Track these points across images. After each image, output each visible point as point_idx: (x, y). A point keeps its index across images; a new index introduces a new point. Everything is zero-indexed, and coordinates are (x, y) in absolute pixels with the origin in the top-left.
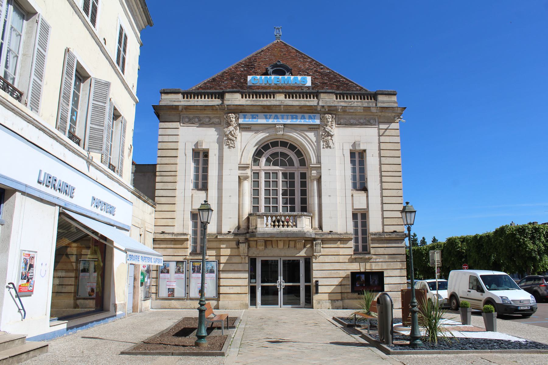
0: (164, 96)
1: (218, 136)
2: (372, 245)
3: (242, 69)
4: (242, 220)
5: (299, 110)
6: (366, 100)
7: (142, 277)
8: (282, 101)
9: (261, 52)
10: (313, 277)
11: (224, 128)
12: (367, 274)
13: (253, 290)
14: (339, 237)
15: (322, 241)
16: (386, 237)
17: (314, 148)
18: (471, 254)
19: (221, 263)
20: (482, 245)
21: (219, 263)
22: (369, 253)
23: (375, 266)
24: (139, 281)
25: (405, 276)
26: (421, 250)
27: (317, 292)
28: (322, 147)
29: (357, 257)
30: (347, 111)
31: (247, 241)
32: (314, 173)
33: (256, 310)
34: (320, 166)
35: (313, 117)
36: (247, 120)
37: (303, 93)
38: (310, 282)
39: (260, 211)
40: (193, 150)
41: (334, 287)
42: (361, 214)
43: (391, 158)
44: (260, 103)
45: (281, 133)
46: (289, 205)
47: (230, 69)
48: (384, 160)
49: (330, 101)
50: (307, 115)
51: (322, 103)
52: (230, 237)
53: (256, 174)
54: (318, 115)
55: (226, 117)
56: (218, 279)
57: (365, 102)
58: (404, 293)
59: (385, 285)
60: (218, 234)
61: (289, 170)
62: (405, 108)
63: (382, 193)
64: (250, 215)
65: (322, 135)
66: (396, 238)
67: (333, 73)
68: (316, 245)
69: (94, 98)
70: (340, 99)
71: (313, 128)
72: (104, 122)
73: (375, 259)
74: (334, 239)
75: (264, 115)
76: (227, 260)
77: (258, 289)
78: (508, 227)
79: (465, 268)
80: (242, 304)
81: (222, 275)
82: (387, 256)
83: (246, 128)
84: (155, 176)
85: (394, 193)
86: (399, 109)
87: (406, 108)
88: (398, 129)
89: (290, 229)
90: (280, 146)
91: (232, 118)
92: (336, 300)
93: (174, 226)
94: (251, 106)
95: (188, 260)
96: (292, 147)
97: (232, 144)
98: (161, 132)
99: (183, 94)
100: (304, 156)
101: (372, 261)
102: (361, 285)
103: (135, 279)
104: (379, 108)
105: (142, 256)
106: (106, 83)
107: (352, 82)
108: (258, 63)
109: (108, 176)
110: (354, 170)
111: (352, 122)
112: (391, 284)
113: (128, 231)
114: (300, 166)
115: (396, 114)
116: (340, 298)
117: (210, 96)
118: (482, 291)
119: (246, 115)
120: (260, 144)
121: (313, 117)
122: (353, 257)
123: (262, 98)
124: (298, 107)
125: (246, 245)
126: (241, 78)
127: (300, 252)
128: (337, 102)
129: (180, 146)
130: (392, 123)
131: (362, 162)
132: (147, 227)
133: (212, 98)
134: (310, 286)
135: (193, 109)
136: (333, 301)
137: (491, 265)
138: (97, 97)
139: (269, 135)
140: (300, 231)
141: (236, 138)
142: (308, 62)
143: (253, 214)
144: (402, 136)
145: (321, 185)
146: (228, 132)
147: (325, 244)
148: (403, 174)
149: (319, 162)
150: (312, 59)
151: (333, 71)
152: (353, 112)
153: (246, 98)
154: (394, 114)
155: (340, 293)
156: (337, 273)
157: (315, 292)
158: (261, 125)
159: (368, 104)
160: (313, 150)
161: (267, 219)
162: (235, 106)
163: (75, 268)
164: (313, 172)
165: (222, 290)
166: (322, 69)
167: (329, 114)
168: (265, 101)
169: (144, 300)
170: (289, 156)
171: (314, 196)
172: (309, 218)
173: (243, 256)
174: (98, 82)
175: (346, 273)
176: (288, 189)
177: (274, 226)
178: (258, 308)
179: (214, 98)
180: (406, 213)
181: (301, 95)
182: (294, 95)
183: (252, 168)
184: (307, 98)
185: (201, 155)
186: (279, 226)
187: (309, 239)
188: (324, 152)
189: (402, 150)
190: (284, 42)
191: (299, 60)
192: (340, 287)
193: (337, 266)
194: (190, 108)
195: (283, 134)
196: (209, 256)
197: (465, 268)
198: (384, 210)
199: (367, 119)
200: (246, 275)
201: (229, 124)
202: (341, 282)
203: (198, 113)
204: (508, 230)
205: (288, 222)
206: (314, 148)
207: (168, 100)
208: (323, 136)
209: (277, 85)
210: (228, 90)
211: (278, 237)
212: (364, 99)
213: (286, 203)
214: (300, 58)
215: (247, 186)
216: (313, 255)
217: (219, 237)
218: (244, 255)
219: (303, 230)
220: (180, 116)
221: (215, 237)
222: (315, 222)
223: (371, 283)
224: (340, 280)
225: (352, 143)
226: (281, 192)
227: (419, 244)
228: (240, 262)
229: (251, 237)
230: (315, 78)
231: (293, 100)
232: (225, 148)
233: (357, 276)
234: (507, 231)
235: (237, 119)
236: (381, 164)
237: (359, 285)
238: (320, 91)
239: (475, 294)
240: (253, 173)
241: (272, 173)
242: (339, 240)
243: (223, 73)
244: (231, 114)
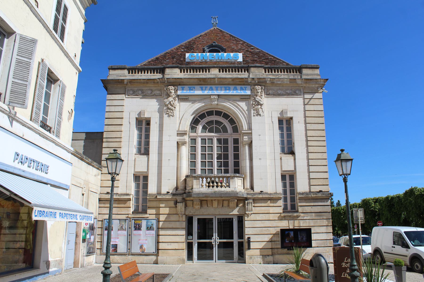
0: (112, 72)
2: (299, 204)
3: (182, 50)
4: (180, 181)
6: (292, 73)
7: (84, 234)
9: (200, 37)
10: (246, 234)
11: (165, 99)
12: (296, 231)
13: (190, 246)
14: (269, 197)
15: (253, 200)
16: (313, 196)
17: (246, 116)
18: (383, 212)
19: (160, 221)
20: (393, 205)
21: (159, 221)
22: (297, 212)
23: (303, 224)
24: (80, 238)
25: (331, 233)
26: (340, 210)
27: (249, 248)
28: (252, 115)
29: (286, 215)
30: (275, 83)
31: (184, 200)
32: (246, 138)
33: (192, 265)
34: (251, 132)
35: (244, 89)
37: (235, 67)
38: (243, 239)
39: (197, 173)
40: (137, 119)
41: (265, 243)
42: (289, 175)
43: (315, 124)
44: (197, 77)
45: (216, 103)
46: (223, 168)
47: (172, 50)
48: (309, 127)
49: (259, 74)
50: (238, 87)
51: (253, 76)
52: (169, 197)
53: (194, 140)
54: (249, 87)
55: (166, 89)
56: (158, 235)
57: (291, 75)
58: (336, 251)
59: (312, 241)
60: (158, 194)
61: (223, 136)
62: (327, 80)
63: (308, 156)
64: (187, 176)
65: (253, 104)
66: (322, 197)
68: (248, 204)
69: (18, 53)
70: (268, 72)
71: (244, 98)
72: (28, 77)
73: (303, 217)
74: (264, 199)
76: (166, 218)
77: (195, 245)
78: (416, 188)
79: (380, 225)
80: (179, 259)
81: (161, 232)
82: (313, 214)
83: (184, 99)
84: (103, 142)
85: (319, 156)
86: (322, 80)
87: (328, 79)
88: (321, 99)
89: (223, 189)
91: (172, 90)
92: (267, 255)
93: (118, 187)
94: (189, 79)
95: (130, 218)
96: (226, 116)
97: (171, 113)
98: (108, 103)
99: (129, 70)
100: (237, 124)
101: (300, 218)
102: (290, 241)
103: (77, 236)
104: (303, 80)
105: (60, 213)
106: (32, 40)
107: (279, 59)
108: (196, 45)
109: (40, 134)
110: (282, 136)
111: (279, 93)
112: (318, 240)
113: (67, 190)
114: (233, 132)
115: (319, 85)
116: (271, 254)
117: (152, 71)
118: (407, 247)
119: (184, 87)
120: (197, 113)
121: (244, 89)
122: (282, 215)
124: (230, 80)
125: (183, 204)
126: (181, 57)
127: (233, 211)
128: (266, 76)
129: (125, 115)
130: (316, 93)
131: (289, 129)
132: (91, 188)
133: (154, 73)
134: (242, 242)
135: (137, 83)
136: (264, 256)
137: (402, 222)
138: (22, 52)
139: (205, 105)
140: (233, 191)
141: (175, 107)
142: (240, 44)
143: (190, 175)
144: (324, 104)
145: (252, 147)
146: (168, 103)
147: (257, 203)
148: (326, 138)
149: (250, 128)
150: (244, 42)
151: (262, 51)
152: (280, 84)
153: (184, 72)
154: (317, 85)
155: (271, 249)
156: (268, 230)
157: (247, 248)
158: (198, 96)
159: (294, 76)
160: (245, 117)
161: (202, 180)
162: (174, 79)
163: (26, 226)
164: (245, 137)
165: (161, 246)
166: (252, 49)
167: (259, 86)
168: (201, 75)
169: (87, 256)
170: (223, 123)
171: (246, 159)
172: (241, 179)
173: (180, 214)
174: (22, 38)
175: (276, 230)
176: (223, 153)
177: (209, 186)
178: (195, 263)
179: (156, 73)
180: (341, 162)
181: (234, 70)
183: (190, 135)
184: (239, 72)
185: (144, 123)
186: (213, 187)
187: (241, 198)
188: (255, 120)
189: (326, 116)
190: (220, 29)
191: (232, 42)
192: (270, 243)
193: (268, 224)
194: (134, 81)
195: (217, 104)
196: (149, 214)
197: (380, 225)
198: (310, 171)
199: (293, 90)
200: (183, 232)
201: (168, 96)
202: (271, 238)
203: (142, 86)
204: (417, 191)
205: (221, 183)
206: (246, 116)
207: (114, 75)
208: (254, 105)
209: (212, 61)
210: (168, 66)
211: (212, 197)
213: (221, 166)
214: (233, 41)
215: (185, 150)
216: (245, 214)
217: (158, 197)
218: (182, 214)
219: (235, 190)
220: (126, 89)
221: (154, 197)
222: (246, 183)
223: (300, 239)
224: (271, 236)
226: (215, 156)
227: (335, 206)
228: (178, 220)
229: (187, 197)
230: (246, 57)
231: (226, 74)
232: (165, 116)
233: (287, 232)
234: (416, 192)
235: (176, 91)
236: (306, 130)
237: (288, 242)
238: (250, 65)
239: (399, 249)
240: (191, 139)
241: (208, 139)
242: (269, 200)
243: (166, 53)
244: (170, 87)
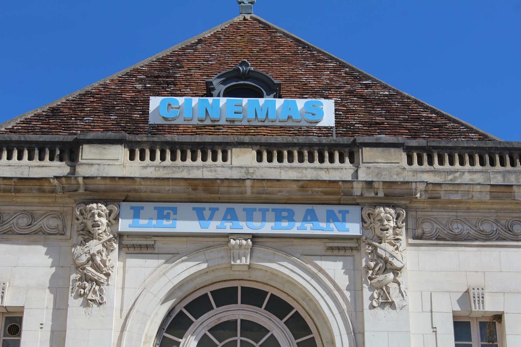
1: (53, 270)
3: (139, 86)
5: (298, 196)
6: (498, 167)
8: (247, 168)
9: (197, 43)
11: (74, 246)
17: (344, 307)
28: (367, 303)
30: (443, 197)
35: (340, 216)
36: (142, 222)
37: (310, 146)
42: (481, 323)
44: (185, 175)
45: (245, 261)
47: (105, 86)
50: (321, 210)
51: (368, 174)
55: (82, 214)
57: (496, 172)
65: (368, 268)
67: (399, 97)
70: (420, 163)
71: (339, 248)
75: (194, 209)
83: (140, 246)
90: (242, 303)
91: (100, 215)
94: (157, 183)
97: (95, 293)
100: (315, 334)
107: (455, 121)
111: (456, 231)
119: (142, 208)
120: (180, 294)
121: (340, 216)
123: (189, 159)
124: (294, 187)
128: (410, 174)
139: (208, 267)
141: (108, 275)
142: (328, 69)
146: (84, 258)
150: (340, 62)
151: (398, 93)
152: (460, 202)
153: (142, 158)
158: (185, 239)
159: (504, 177)
160: (341, 312)
162: (108, 182)
166: (367, 86)
168: (198, 167)
170: (268, 331)
179: (47, 157)
181: (306, 153)
182: (286, 153)
184: (322, 161)
191: (302, 65)
195: (249, 267)
199: (503, 222)
206: (344, 307)
208: (370, 272)
209: (236, 123)
210: (91, 136)
212: (493, 163)
214: (306, 59)
225: (461, 294)
238: (360, 139)
243: (84, 95)
244: (94, 205)
